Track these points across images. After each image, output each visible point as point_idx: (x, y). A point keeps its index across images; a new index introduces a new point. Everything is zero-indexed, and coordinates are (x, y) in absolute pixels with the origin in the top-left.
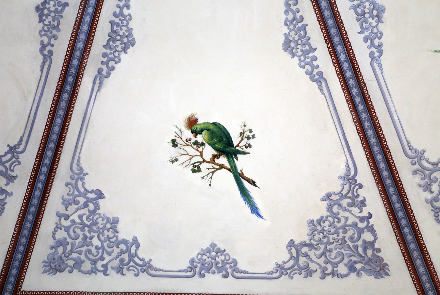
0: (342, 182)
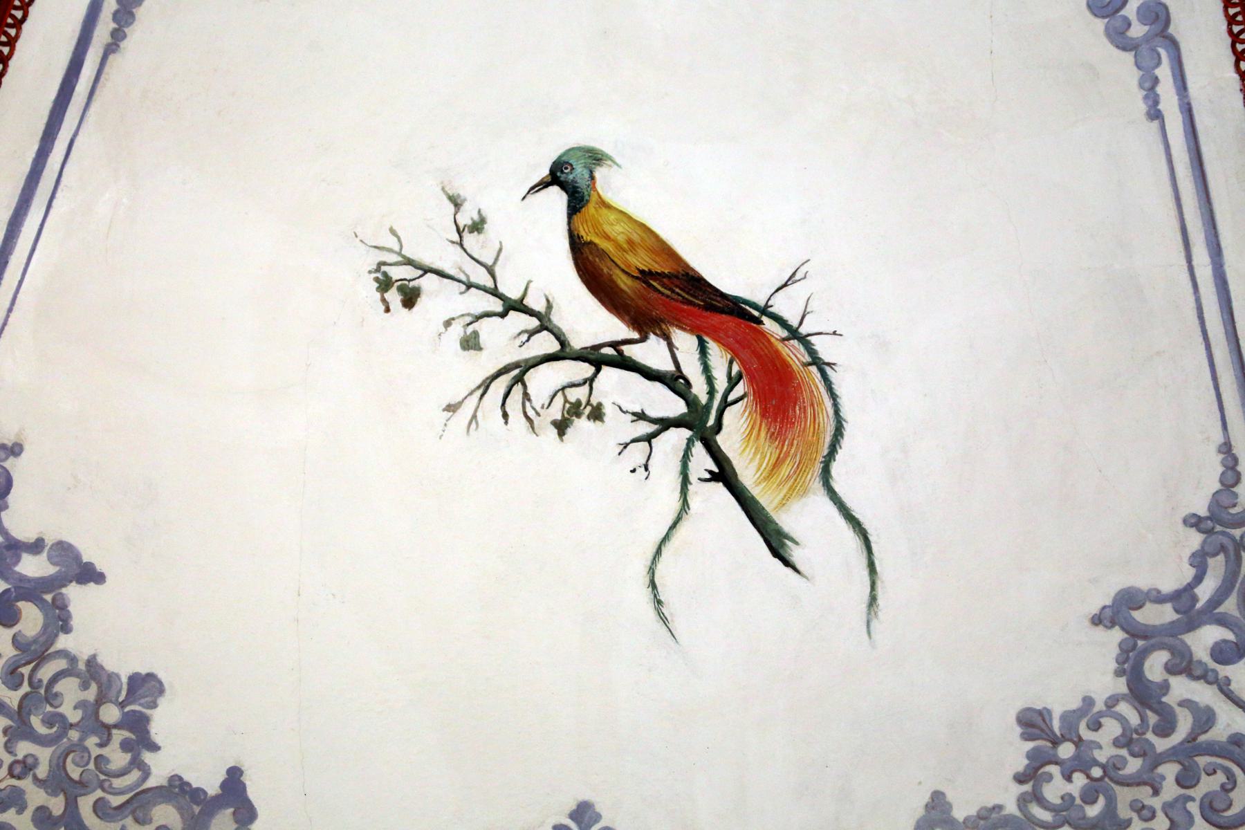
0: (1195, 540)
